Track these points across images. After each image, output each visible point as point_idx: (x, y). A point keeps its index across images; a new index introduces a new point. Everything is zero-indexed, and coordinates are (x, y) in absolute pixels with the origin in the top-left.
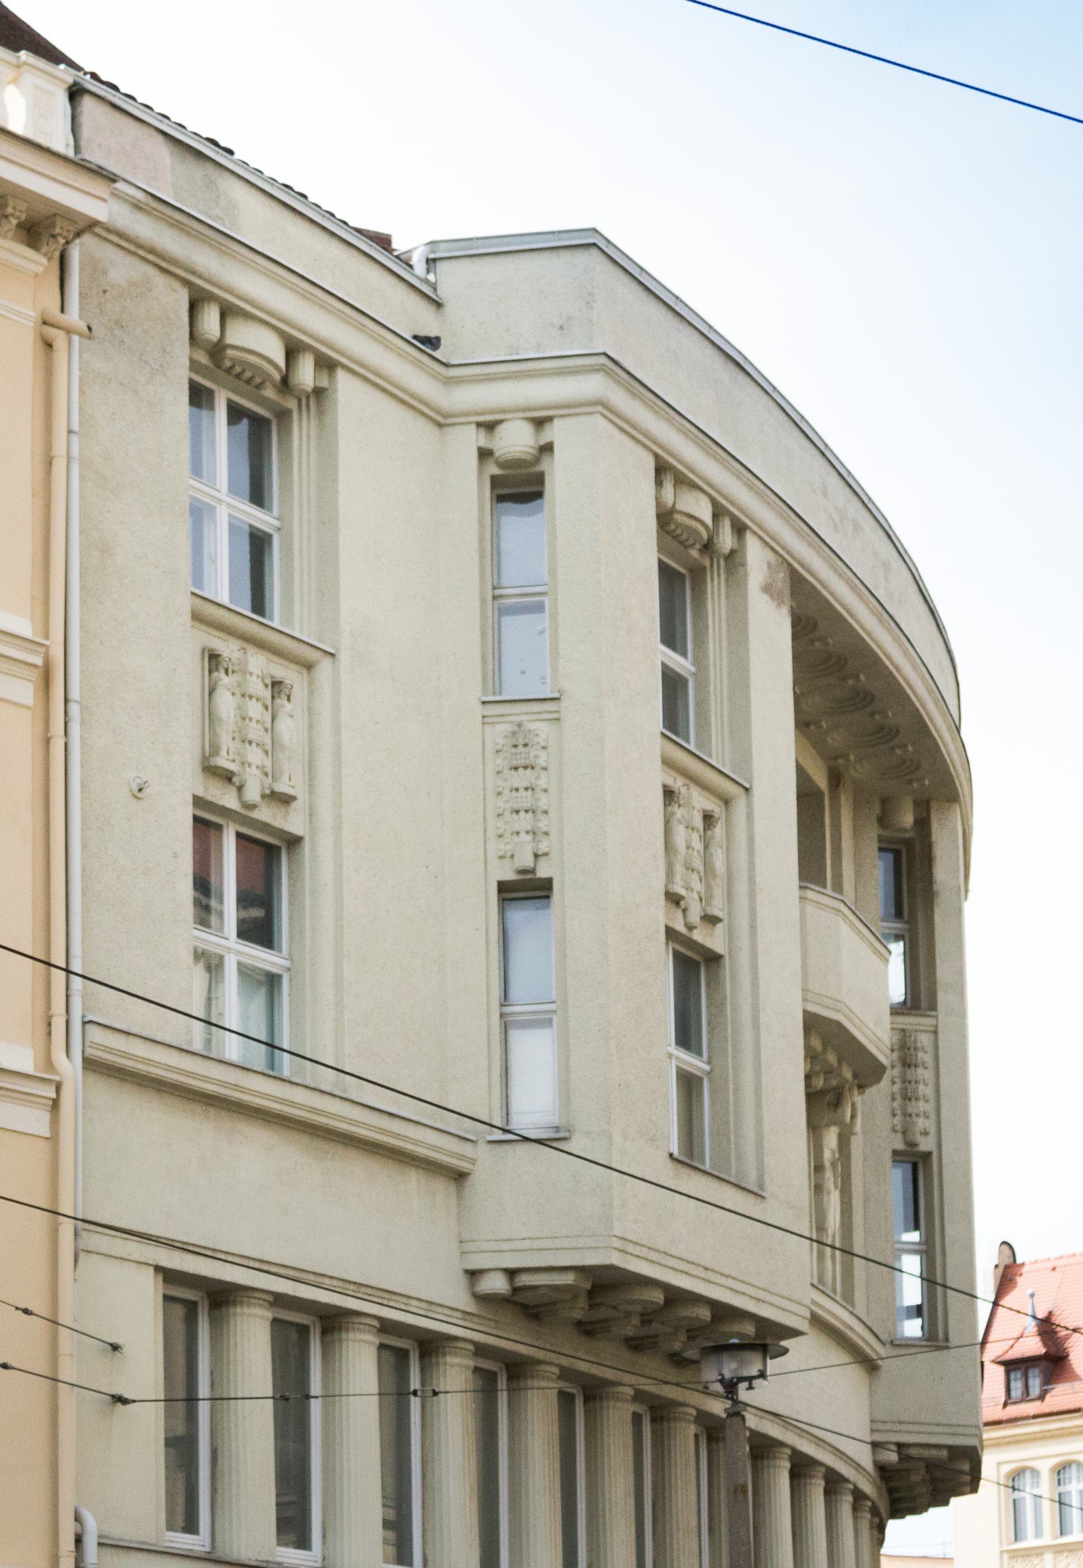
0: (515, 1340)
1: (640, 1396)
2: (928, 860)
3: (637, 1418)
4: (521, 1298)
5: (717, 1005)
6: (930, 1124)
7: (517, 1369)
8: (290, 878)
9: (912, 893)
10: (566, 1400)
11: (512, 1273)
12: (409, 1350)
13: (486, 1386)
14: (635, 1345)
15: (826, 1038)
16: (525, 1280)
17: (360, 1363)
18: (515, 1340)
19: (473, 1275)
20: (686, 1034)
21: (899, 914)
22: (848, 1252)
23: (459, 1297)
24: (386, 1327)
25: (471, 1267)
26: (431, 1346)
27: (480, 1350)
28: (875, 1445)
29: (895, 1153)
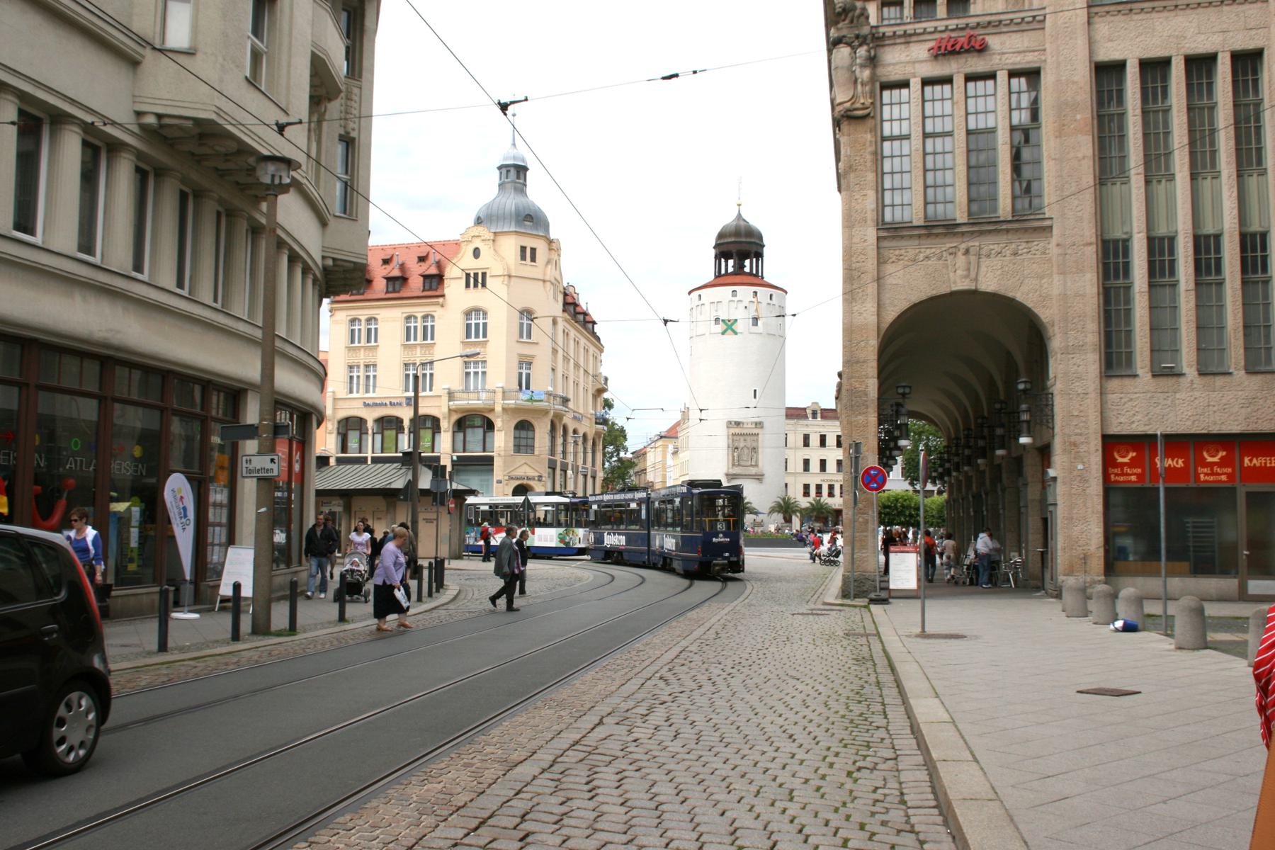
0: (161, 156)
1: (220, 201)
2: (363, 16)
3: (219, 214)
4: (163, 132)
5: (272, 23)
6: (356, 126)
7: (160, 172)
8: (154, 211)
9: (355, 30)
10: (183, 197)
11: (159, 116)
12: (99, 148)
13: (142, 175)
14: (222, 174)
15: (319, 67)
16: (167, 121)
17: (71, 148)
18: (161, 156)
19: (139, 114)
20: (257, 30)
21: (348, 37)
22: (318, 163)
23: (126, 117)
24: (88, 128)
25: (137, 109)
26: (115, 147)
27: (139, 155)
28: (324, 258)
29: (340, 136)
